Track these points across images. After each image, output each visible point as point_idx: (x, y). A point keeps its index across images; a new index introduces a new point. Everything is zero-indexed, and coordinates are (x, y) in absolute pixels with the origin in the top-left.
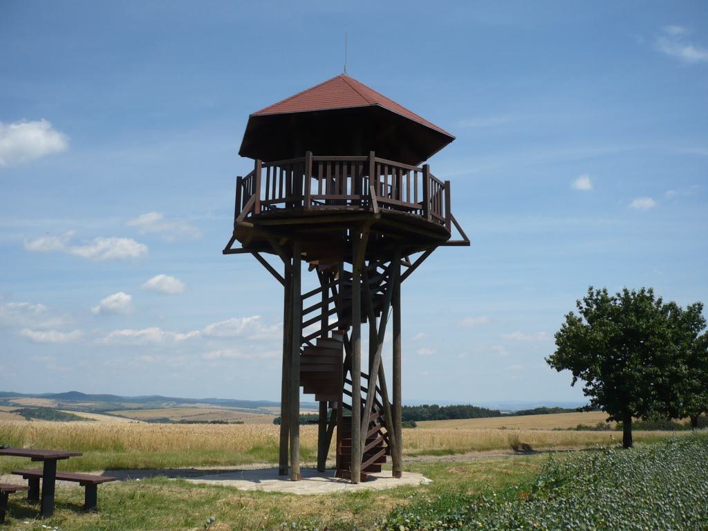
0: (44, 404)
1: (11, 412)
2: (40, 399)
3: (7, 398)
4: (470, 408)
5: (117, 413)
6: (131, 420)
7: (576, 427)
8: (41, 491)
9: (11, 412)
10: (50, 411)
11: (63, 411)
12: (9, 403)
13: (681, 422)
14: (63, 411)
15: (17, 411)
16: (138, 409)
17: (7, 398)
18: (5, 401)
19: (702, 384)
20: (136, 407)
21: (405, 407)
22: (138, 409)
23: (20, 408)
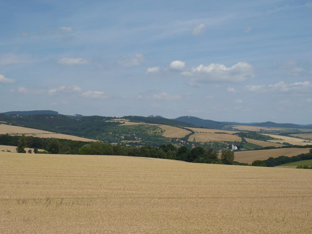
0: (252, 129)
1: (233, 134)
2: (250, 126)
3: (231, 126)
4: (273, 147)
5: (296, 135)
6: (304, 140)
7: (252, 164)
8: (90, 140)
9: (233, 134)
10: (256, 134)
11: (262, 134)
12: (232, 129)
13: (11, 124)
14: (262, 134)
15: (237, 134)
16: (309, 133)
17: (231, 126)
18: (230, 127)
19: (189, 142)
20: (308, 132)
21: (197, 142)
22: (309, 133)
23: (238, 132)
